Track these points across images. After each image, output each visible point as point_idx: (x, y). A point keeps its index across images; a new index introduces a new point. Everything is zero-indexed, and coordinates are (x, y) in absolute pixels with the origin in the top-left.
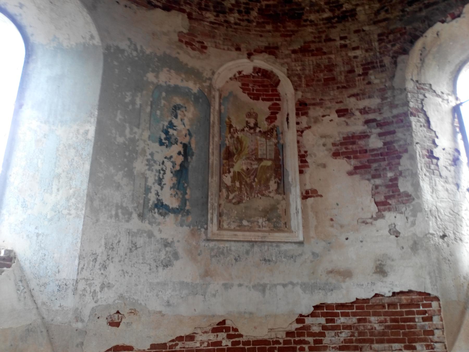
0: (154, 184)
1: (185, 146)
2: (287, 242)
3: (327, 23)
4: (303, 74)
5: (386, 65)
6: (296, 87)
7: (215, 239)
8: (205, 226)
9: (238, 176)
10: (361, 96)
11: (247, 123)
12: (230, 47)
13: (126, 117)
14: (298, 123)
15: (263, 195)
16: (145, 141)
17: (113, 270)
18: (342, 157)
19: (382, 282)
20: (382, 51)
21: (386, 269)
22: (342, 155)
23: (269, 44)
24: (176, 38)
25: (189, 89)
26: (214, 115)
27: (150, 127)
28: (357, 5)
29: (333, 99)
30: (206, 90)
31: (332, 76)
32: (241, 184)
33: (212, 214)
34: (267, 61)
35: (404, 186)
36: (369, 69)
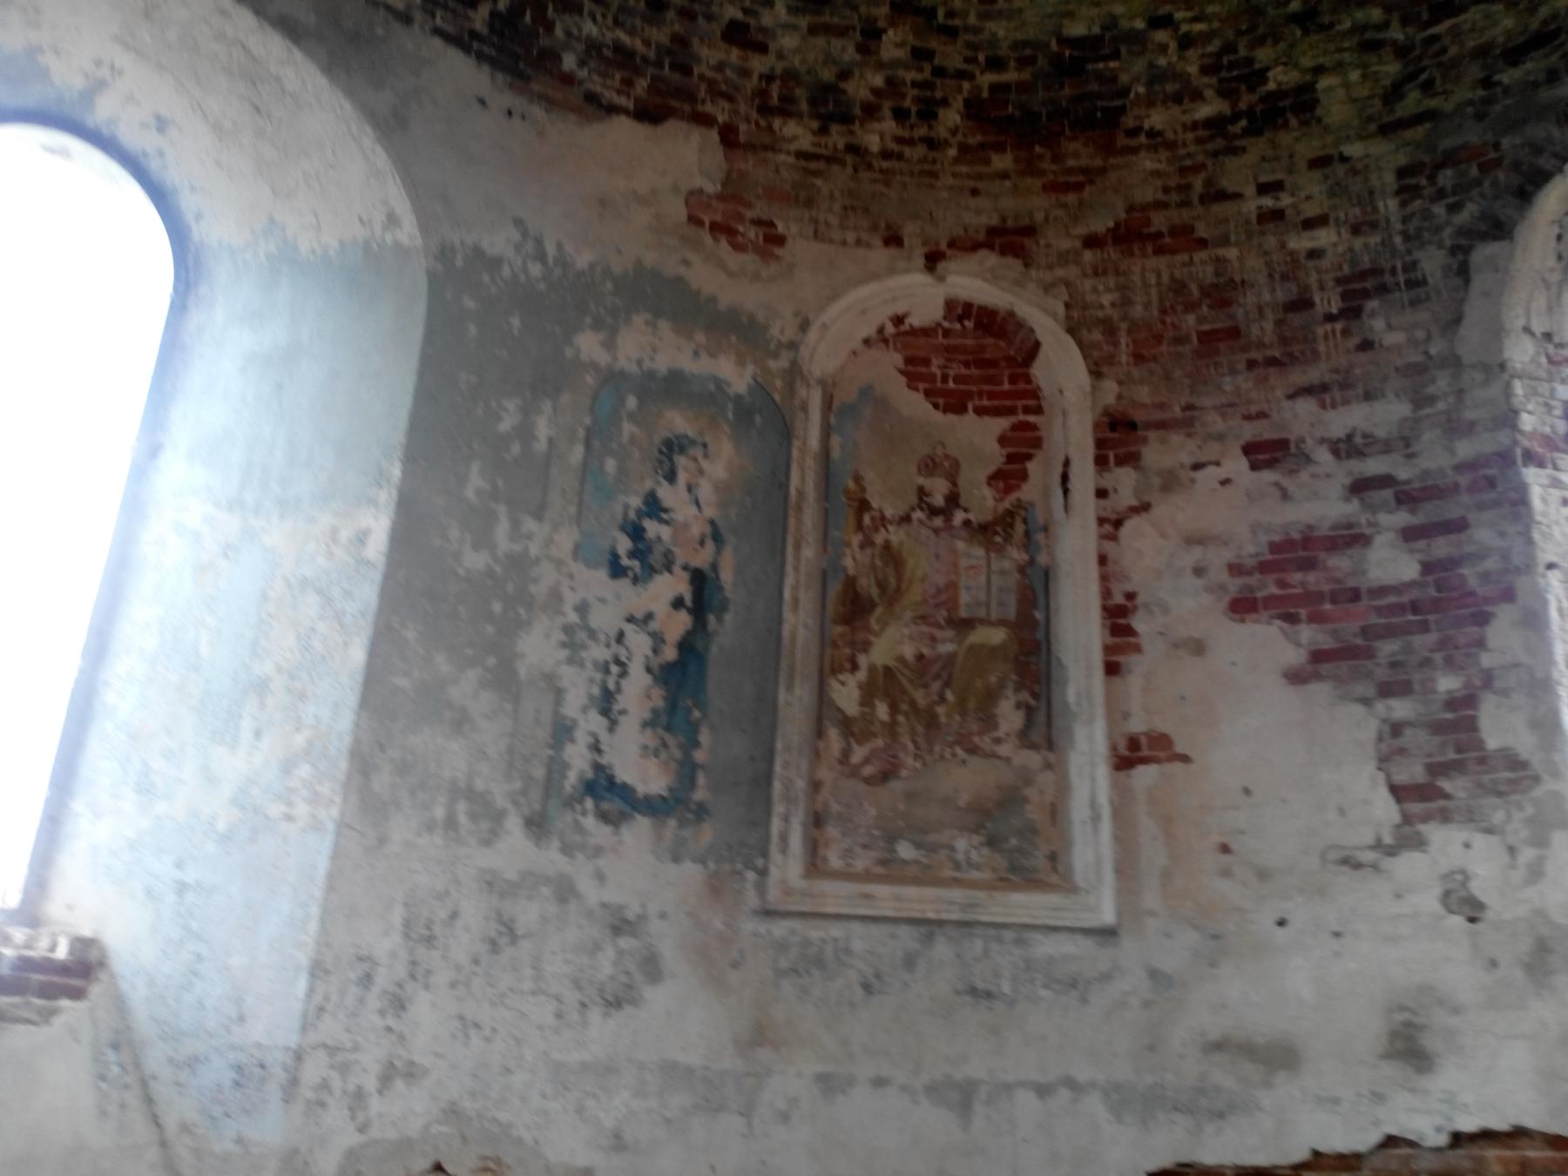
0: (584, 710)
1: (699, 579)
2: (1055, 929)
3: (1212, 138)
4: (1124, 318)
5: (1430, 281)
6: (1096, 364)
7: (793, 908)
8: (760, 862)
9: (884, 684)
10: (1337, 394)
11: (922, 492)
12: (864, 236)
13: (500, 483)
14: (1101, 493)
15: (973, 750)
16: (559, 563)
17: (428, 1014)
18: (1265, 615)
19: (1413, 1090)
20: (1411, 228)
21: (1429, 1042)
22: (1266, 608)
23: (1004, 220)
24: (681, 213)
25: (719, 382)
26: (802, 469)
27: (580, 513)
28: (1319, 70)
29: (1232, 405)
30: (779, 383)
31: (1230, 323)
32: (894, 709)
33: (786, 819)
34: (994, 277)
35: (1500, 727)
36: (1366, 294)
